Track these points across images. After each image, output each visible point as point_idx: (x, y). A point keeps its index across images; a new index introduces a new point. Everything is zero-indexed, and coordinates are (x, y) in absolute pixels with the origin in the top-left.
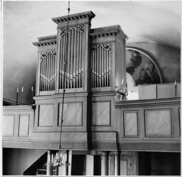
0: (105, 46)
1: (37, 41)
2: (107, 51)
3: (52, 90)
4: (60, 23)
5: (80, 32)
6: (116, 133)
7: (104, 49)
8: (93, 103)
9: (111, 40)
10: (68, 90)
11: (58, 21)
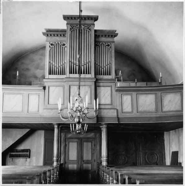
0: (106, 44)
1: (45, 31)
2: (108, 48)
3: (62, 74)
4: (69, 20)
5: (86, 30)
6: (116, 110)
7: (61, 46)
8: (97, 87)
9: (111, 40)
10: (83, 76)
11: (66, 18)
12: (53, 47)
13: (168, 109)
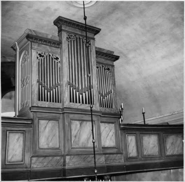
0: (106, 67)
12: (41, 60)
13: (171, 153)
